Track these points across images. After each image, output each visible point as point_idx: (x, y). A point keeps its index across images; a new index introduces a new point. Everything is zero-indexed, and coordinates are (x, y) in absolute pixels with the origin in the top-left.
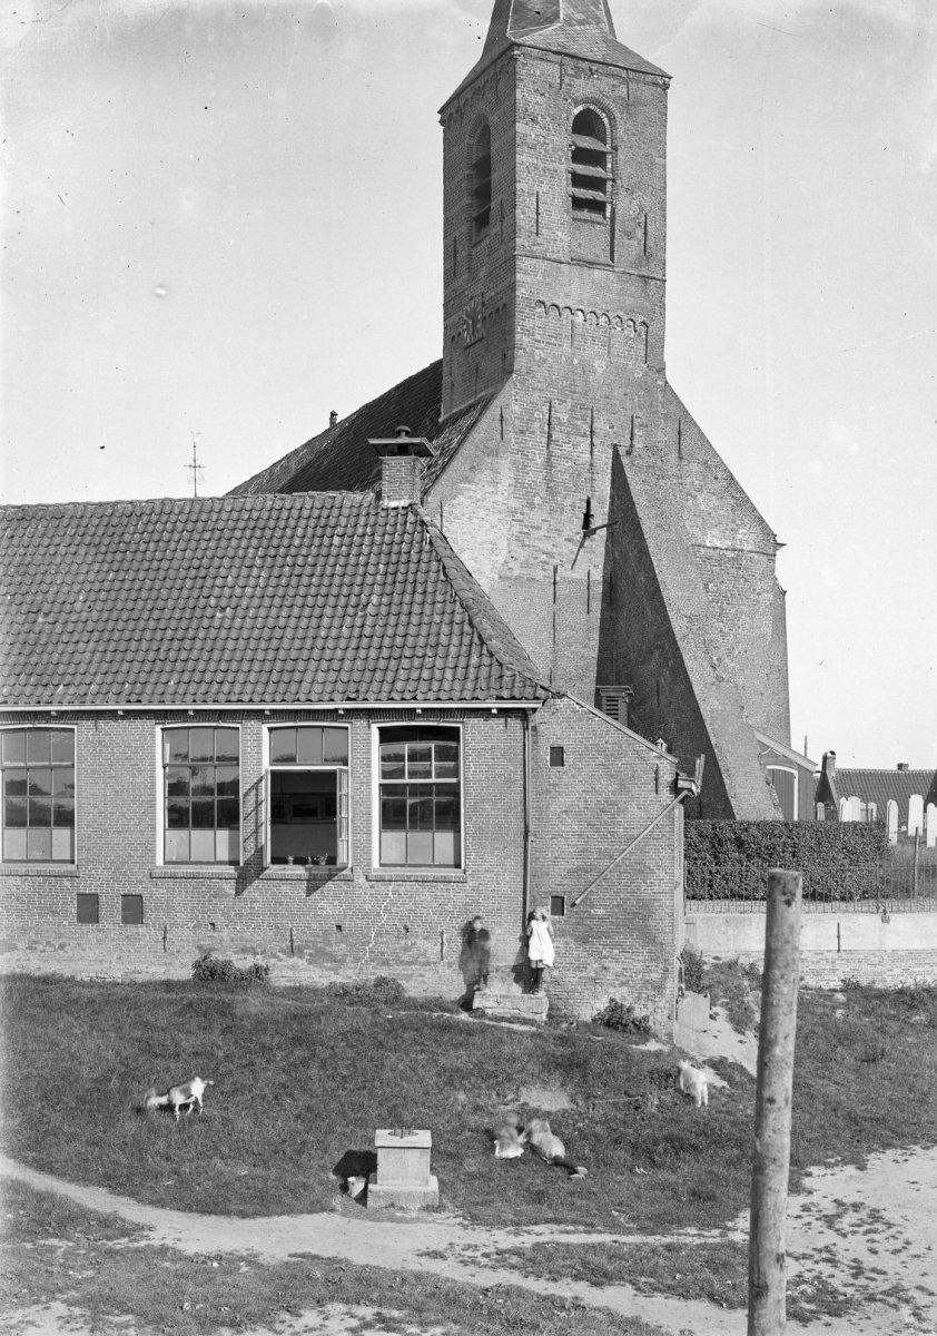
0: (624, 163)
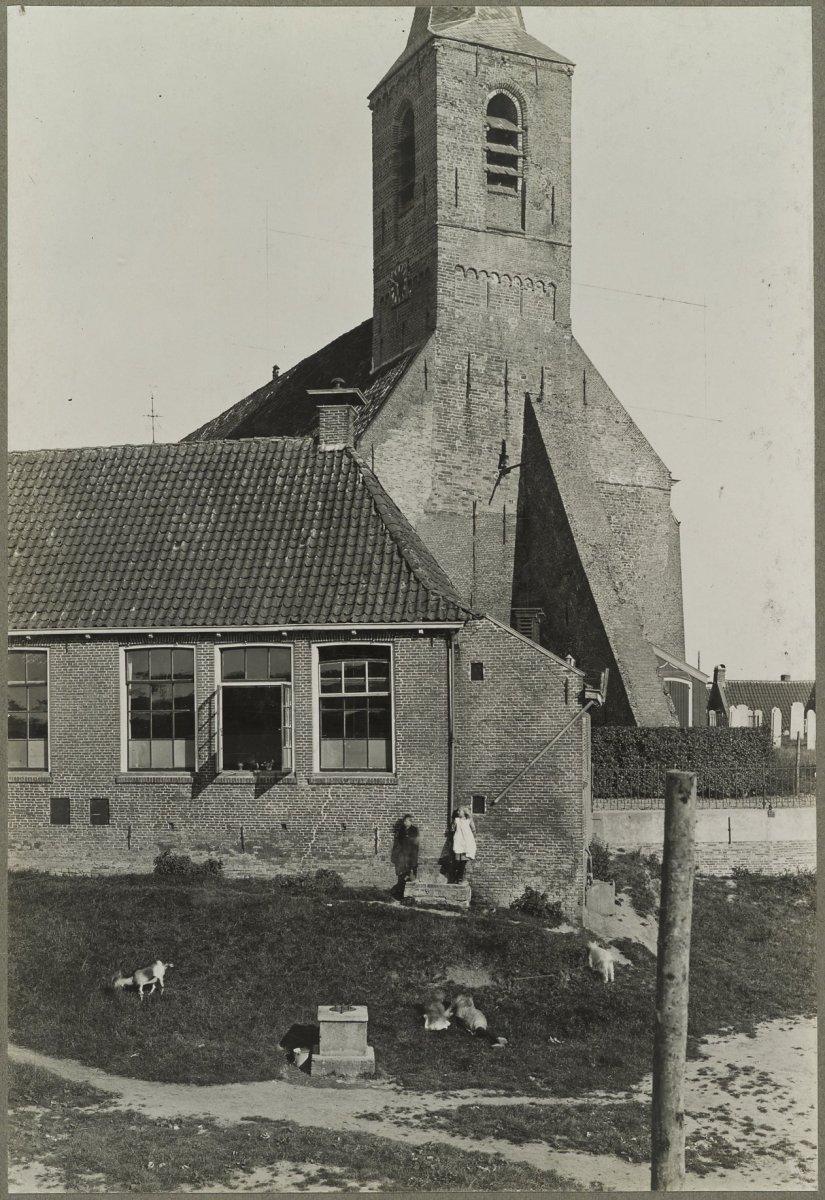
0: (534, 143)
